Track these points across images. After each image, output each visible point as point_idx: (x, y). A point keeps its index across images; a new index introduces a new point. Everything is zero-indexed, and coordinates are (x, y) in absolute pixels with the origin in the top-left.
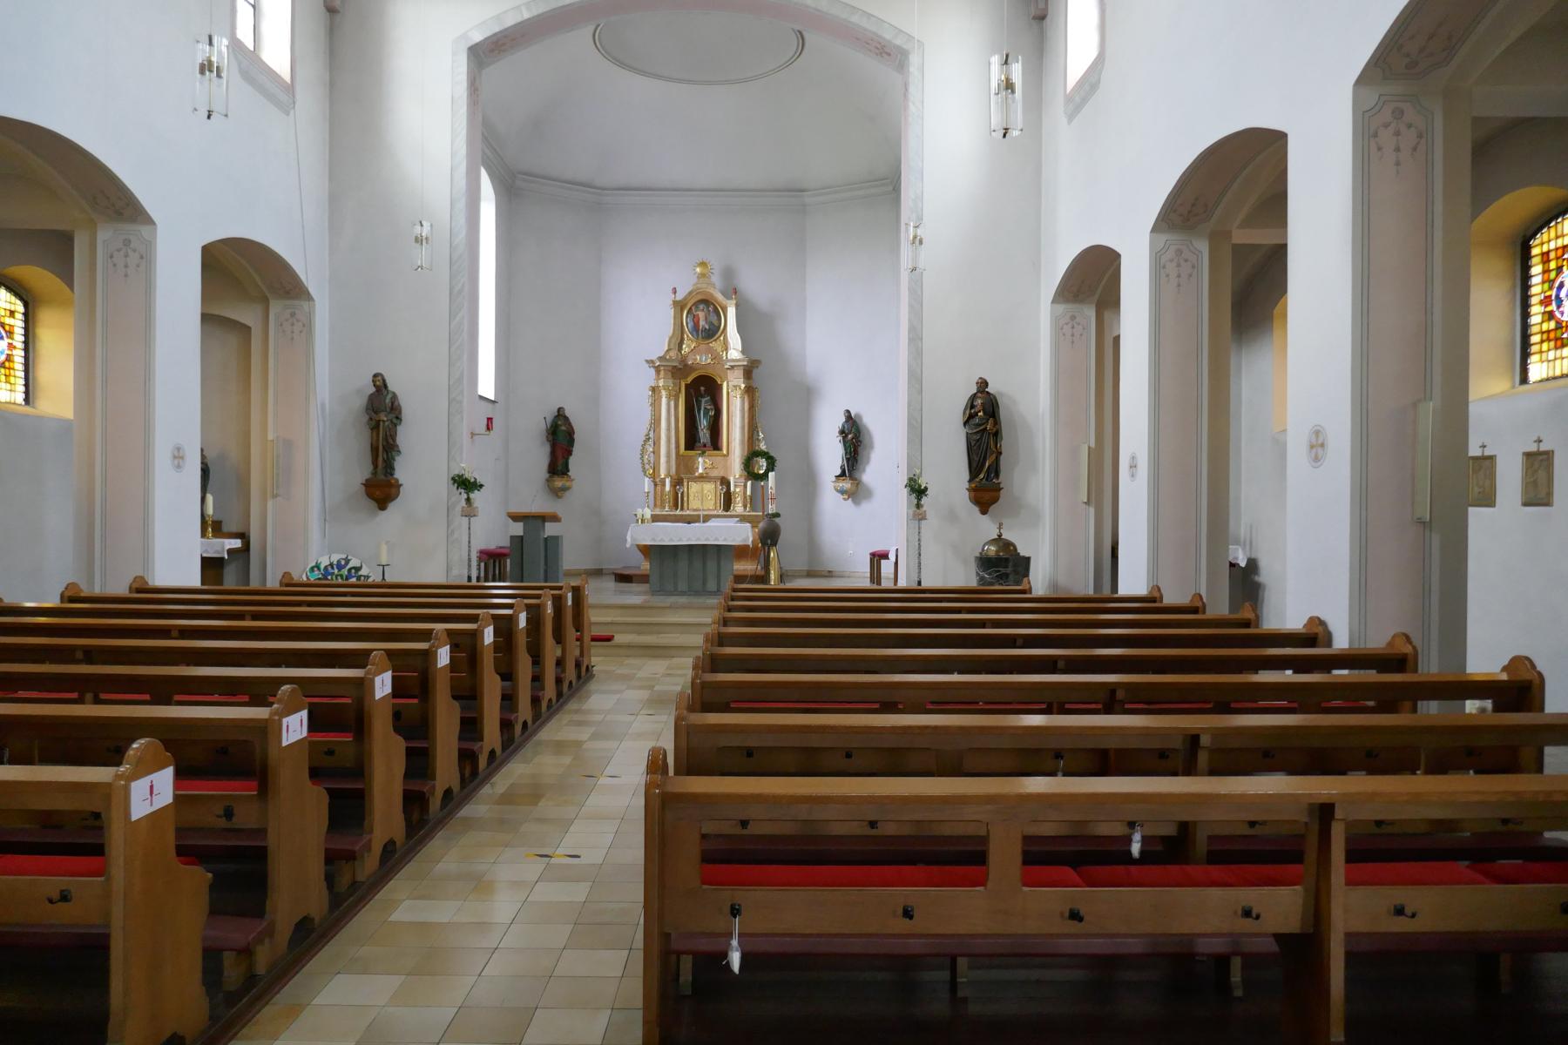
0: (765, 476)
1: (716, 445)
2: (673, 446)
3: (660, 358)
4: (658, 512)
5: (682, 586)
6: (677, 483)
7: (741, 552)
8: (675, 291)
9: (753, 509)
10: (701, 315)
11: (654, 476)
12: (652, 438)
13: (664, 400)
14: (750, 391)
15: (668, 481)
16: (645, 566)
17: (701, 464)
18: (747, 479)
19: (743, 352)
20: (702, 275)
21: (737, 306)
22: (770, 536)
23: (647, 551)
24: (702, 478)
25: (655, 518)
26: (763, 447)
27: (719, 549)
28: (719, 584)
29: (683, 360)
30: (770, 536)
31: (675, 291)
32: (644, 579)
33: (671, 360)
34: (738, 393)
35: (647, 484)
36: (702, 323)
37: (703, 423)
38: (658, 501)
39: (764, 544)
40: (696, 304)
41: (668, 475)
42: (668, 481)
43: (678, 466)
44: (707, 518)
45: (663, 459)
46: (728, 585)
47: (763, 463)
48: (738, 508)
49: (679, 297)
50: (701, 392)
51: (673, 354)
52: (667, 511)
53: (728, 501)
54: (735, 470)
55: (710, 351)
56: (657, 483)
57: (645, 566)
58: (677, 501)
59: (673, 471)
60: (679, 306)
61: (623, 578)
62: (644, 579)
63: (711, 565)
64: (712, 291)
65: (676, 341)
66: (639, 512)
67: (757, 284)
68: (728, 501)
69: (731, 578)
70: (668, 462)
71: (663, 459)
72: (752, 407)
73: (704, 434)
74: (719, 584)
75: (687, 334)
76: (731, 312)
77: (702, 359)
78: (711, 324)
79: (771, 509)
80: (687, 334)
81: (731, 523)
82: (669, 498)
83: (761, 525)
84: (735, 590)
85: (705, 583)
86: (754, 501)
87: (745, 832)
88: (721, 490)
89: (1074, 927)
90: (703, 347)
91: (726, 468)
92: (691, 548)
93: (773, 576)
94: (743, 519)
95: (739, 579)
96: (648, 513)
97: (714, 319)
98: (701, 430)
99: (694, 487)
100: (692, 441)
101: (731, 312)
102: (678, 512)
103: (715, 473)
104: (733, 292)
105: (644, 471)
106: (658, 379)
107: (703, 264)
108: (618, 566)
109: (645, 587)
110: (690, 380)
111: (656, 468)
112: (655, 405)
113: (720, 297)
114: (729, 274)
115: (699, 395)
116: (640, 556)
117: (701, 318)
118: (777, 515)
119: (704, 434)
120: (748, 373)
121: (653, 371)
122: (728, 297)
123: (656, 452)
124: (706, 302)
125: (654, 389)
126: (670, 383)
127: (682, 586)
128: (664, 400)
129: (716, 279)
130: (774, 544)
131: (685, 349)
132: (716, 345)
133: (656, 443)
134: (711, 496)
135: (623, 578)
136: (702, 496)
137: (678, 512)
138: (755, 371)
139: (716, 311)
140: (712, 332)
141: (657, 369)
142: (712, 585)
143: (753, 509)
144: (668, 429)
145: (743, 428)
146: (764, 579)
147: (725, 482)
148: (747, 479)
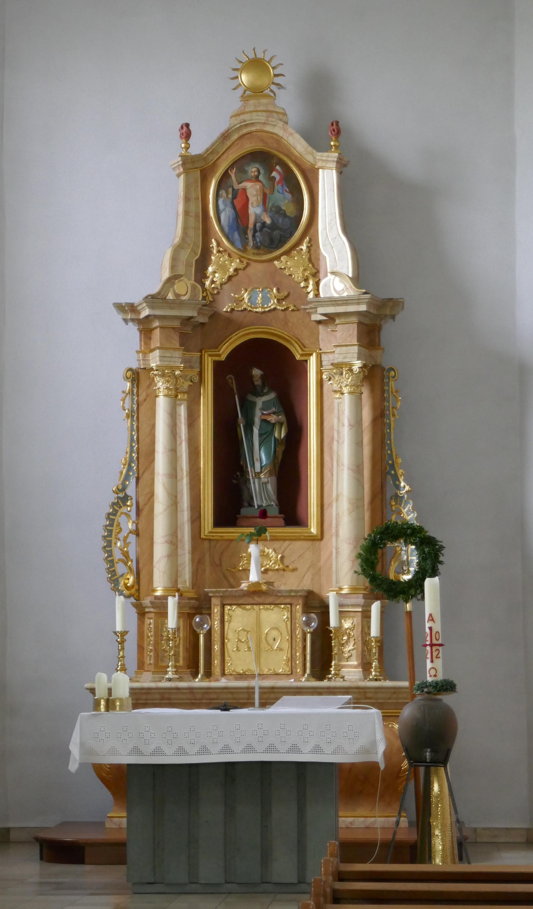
0: (415, 588)
1: (290, 508)
2: (185, 516)
3: (153, 300)
4: (147, 681)
5: (210, 869)
6: (196, 607)
7: (355, 782)
8: (186, 133)
9: (386, 672)
10: (253, 190)
11: (137, 593)
12: (131, 498)
13: (162, 404)
14: (375, 376)
15: (172, 603)
16: (117, 820)
17: (256, 561)
18: (370, 598)
19: (357, 280)
20: (255, 92)
21: (342, 166)
22: (429, 741)
23: (122, 780)
24: (259, 595)
25: (141, 699)
26: (409, 515)
27: (302, 774)
28: (302, 867)
29: (209, 303)
30: (429, 741)
31: (186, 133)
32: (113, 853)
33: (178, 303)
34: (346, 382)
35: (121, 613)
36: (255, 210)
37: (260, 458)
38: (150, 653)
39: (415, 760)
40: (240, 164)
41: (174, 588)
42: (172, 603)
43: (197, 563)
44: (270, 697)
45: (160, 550)
46: (323, 864)
47: (410, 555)
48: (349, 670)
49: (199, 145)
50: (250, 383)
51: (183, 288)
52: (170, 679)
53: (322, 654)
54: (340, 573)
55: (277, 279)
56: (146, 608)
57: (117, 820)
58: (197, 654)
59: (186, 578)
60: (199, 169)
61: (61, 852)
62: (113, 853)
63: (283, 815)
64: (278, 130)
65: (189, 256)
66: (101, 682)
67: (388, 111)
68: (322, 654)
69: (332, 845)
70: (173, 555)
71: (160, 550)
72: (380, 417)
73: (262, 487)
74: (302, 867)
75: (219, 238)
76: (328, 181)
77: (256, 300)
78: (278, 211)
79: (432, 670)
80: (219, 238)
81: (330, 708)
82: (175, 650)
83: (407, 712)
84: (341, 877)
85: (266, 857)
86: (383, 654)
87: (180, 675)
88: (305, 624)
89: (272, 640)
90: (256, 269)
91: (318, 570)
92: (230, 773)
93: (438, 844)
94: (361, 697)
95: (354, 849)
96: (122, 685)
97: (282, 199)
98: (251, 472)
99: (239, 618)
100: (231, 503)
101: (328, 181)
102: (198, 683)
103: (288, 583)
104: (331, 132)
105: (114, 580)
106: (146, 349)
107: (256, 64)
108: (47, 823)
109: (115, 874)
110: (224, 351)
111: (142, 571)
112: (140, 414)
113: (299, 145)
114: (320, 87)
115: (248, 389)
116: (104, 794)
117: (248, 192)
118: (447, 687)
119: (262, 487)
120: (370, 332)
121: (133, 332)
122: (317, 143)
123: (143, 533)
124: (266, 158)
125: (136, 377)
126: (177, 359)
127: (210, 869)
128: (162, 404)
129: (288, 100)
130: (442, 759)
131: (215, 274)
132: (291, 265)
133: (144, 511)
134: (281, 642)
135: (61, 852)
136: (257, 639)
137: (198, 683)
138: (389, 331)
139: (292, 180)
140: (281, 232)
141: (145, 328)
142: (283, 868)
143: (386, 672)
144: (173, 474)
145: (358, 469)
146: (417, 849)
147: (314, 604)
148: (370, 598)
